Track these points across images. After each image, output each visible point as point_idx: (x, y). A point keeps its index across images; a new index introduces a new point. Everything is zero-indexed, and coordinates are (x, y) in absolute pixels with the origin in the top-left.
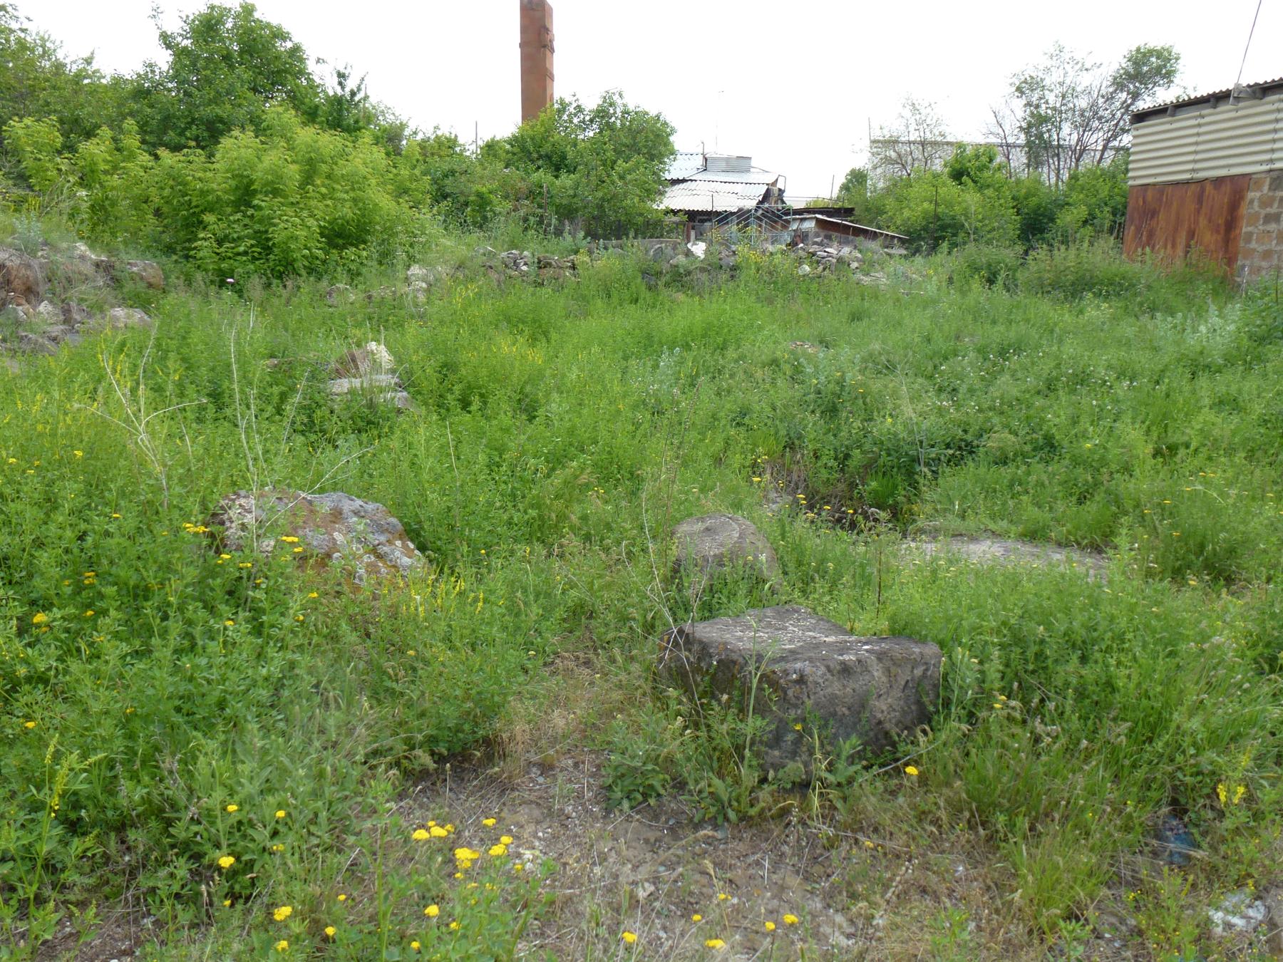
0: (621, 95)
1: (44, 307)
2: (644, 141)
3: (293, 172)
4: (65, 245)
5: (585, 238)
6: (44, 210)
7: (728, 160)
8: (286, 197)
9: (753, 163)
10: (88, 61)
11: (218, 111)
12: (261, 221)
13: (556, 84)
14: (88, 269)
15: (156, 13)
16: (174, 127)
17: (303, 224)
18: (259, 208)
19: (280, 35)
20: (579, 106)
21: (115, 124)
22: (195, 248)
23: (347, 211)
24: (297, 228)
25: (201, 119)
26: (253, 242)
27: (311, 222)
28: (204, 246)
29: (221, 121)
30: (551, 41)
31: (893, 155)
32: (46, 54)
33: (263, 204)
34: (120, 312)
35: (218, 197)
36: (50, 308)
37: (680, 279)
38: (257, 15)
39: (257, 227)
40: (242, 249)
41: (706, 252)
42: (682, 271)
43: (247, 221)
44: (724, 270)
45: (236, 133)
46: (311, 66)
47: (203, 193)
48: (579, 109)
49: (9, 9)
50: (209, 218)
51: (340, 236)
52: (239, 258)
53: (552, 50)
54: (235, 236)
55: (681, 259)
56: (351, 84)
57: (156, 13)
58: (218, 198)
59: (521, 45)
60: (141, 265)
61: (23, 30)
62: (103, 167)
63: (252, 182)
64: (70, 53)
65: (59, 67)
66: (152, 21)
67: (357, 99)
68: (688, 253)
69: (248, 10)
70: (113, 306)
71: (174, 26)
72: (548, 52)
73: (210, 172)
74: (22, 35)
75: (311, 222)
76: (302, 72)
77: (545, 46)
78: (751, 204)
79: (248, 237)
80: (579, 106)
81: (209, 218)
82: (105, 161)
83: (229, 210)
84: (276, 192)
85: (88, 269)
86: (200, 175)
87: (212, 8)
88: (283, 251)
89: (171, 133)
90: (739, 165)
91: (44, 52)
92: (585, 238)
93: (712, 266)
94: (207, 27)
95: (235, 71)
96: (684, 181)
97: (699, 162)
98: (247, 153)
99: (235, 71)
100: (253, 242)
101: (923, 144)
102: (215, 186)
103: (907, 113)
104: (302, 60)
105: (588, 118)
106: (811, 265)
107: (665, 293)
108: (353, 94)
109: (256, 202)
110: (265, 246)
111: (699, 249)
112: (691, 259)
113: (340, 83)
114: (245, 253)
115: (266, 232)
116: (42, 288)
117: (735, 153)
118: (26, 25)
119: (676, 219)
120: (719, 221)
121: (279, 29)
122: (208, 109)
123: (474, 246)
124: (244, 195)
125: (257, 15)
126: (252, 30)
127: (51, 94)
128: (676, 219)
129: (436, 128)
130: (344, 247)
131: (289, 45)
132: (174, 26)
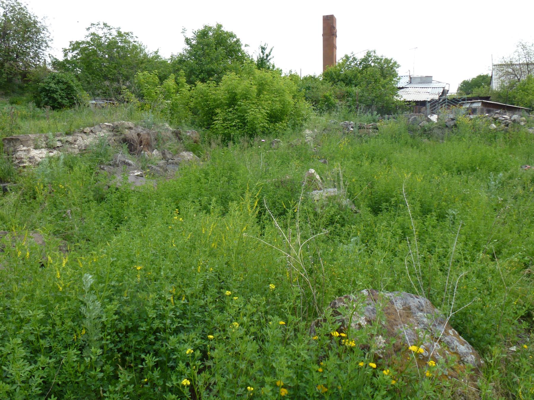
0: (375, 52)
1: (155, 152)
2: (386, 71)
3: (254, 89)
4: (161, 124)
5: (377, 114)
6: (153, 109)
7: (421, 78)
8: (251, 100)
9: (433, 79)
10: (156, 53)
11: (212, 67)
12: (240, 112)
13: (337, 51)
14: (169, 134)
15: (184, 31)
16: (194, 74)
17: (260, 112)
18: (240, 106)
19: (232, 36)
20: (354, 58)
21: (176, 71)
22: (214, 124)
23: (278, 106)
24: (257, 114)
25: (205, 70)
26: (239, 121)
27: (263, 111)
28: (218, 123)
29: (213, 71)
30: (336, 33)
31: (510, 70)
32: (142, 50)
33: (242, 103)
34: (185, 154)
35: (221, 101)
36: (157, 152)
37: (427, 132)
38: (222, 29)
39: (239, 114)
40: (234, 124)
41: (438, 119)
42: (426, 128)
43: (235, 111)
44: (451, 128)
45: (228, 73)
46: (243, 48)
47: (215, 100)
48: (355, 59)
49: (130, 34)
50: (218, 111)
51: (274, 117)
52: (232, 128)
53: (336, 36)
54: (230, 118)
55: (425, 123)
56: (267, 52)
57: (184, 31)
58: (222, 102)
59: (323, 35)
60: (191, 133)
61: (135, 42)
62: (173, 91)
63: (236, 94)
64: (150, 50)
65: (145, 55)
66: (182, 34)
67: (268, 58)
68: (429, 120)
69: (220, 26)
70: (181, 151)
71: (190, 35)
72: (334, 37)
73: (218, 91)
74: (135, 43)
75: (263, 111)
76: (239, 51)
77: (333, 35)
78: (436, 97)
79: (235, 118)
80: (354, 58)
81: (218, 111)
82: (174, 89)
83: (226, 107)
84: (246, 98)
85: (169, 134)
86: (214, 92)
87: (206, 27)
88: (252, 125)
89: (193, 76)
90: (426, 80)
91: (141, 50)
92: (377, 114)
93: (443, 126)
94: (203, 34)
95: (214, 51)
96: (403, 88)
97: (408, 79)
98: (235, 82)
99: (214, 51)
100: (239, 121)
101: (528, 64)
102: (220, 97)
103: (520, 50)
104: (239, 46)
105: (358, 63)
106: (495, 124)
107: (418, 139)
108: (267, 56)
109: (239, 103)
110: (244, 122)
111: (434, 118)
112: (431, 123)
113: (262, 52)
114: (235, 126)
115: (244, 116)
116: (154, 143)
117: (424, 75)
118: (136, 39)
119: (406, 103)
120: (488, 98)
121: (232, 34)
122: (208, 66)
123: (324, 119)
124: (233, 101)
125: (222, 29)
126: (221, 35)
127: (147, 64)
128: (406, 103)
129: (291, 71)
130: (276, 122)
131: (235, 39)
132: (190, 35)
